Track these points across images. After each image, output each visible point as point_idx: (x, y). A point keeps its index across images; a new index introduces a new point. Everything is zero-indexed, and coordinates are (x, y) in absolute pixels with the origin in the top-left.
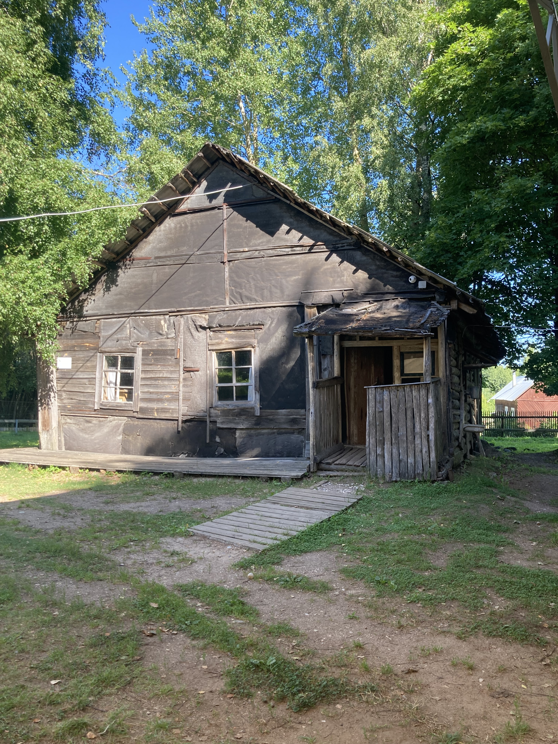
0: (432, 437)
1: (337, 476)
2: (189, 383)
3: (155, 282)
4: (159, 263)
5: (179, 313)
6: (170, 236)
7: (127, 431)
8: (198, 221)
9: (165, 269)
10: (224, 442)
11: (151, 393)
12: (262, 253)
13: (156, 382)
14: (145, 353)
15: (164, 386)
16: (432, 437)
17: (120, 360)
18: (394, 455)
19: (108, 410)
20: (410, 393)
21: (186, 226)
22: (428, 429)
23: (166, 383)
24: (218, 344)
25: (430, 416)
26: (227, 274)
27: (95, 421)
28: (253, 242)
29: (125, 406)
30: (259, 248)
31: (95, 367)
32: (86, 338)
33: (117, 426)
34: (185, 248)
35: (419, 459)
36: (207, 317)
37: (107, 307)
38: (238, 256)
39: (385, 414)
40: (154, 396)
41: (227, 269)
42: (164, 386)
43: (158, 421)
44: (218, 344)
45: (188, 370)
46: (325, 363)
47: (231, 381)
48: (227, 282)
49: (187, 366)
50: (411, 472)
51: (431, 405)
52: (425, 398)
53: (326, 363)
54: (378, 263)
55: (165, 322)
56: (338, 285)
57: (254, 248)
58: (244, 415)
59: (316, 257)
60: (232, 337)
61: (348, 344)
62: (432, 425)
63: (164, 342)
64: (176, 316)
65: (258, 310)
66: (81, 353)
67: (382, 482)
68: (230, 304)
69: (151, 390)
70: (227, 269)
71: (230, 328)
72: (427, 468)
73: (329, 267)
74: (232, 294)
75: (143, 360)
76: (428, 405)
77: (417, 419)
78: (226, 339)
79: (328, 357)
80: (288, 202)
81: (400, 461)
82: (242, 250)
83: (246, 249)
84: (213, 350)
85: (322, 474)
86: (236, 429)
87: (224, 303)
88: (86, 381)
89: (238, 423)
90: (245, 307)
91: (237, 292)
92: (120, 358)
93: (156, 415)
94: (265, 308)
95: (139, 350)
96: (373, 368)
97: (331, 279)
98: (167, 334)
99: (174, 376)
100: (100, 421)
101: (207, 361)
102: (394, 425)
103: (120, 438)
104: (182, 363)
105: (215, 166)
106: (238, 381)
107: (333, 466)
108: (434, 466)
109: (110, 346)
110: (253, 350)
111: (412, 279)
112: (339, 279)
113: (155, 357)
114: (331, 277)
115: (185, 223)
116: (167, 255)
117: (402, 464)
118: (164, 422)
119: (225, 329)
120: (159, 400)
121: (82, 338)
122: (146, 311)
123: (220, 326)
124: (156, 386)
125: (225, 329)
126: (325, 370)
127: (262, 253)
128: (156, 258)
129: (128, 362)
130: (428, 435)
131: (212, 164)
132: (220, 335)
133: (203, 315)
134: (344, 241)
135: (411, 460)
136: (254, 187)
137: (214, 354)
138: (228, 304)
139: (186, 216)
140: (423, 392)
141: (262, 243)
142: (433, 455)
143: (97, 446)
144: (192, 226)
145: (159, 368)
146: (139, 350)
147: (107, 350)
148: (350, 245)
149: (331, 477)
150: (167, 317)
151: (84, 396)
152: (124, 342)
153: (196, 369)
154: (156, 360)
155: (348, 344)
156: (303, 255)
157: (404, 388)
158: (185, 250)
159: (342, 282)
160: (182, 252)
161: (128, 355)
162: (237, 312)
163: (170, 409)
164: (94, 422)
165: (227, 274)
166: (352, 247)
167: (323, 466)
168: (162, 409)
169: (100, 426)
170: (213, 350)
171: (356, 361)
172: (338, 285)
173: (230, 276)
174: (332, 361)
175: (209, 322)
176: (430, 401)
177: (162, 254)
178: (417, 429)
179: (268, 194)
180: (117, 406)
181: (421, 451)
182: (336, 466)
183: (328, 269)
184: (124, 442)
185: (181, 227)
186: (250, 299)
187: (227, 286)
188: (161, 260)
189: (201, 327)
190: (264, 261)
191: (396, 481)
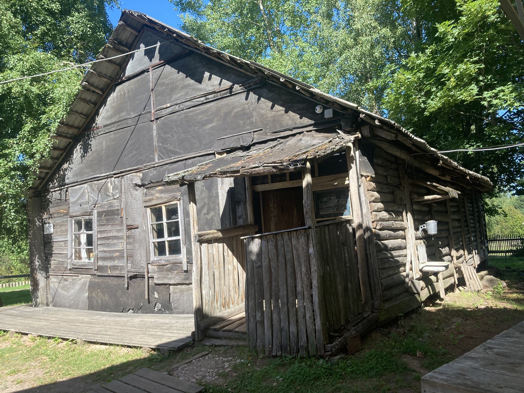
0: (316, 299)
1: (222, 346)
2: (132, 240)
3: (104, 148)
4: (107, 131)
5: (120, 175)
6: (114, 104)
7: (92, 287)
8: (133, 87)
9: (110, 135)
10: (161, 298)
11: (105, 252)
12: (181, 106)
13: (108, 242)
14: (100, 214)
15: (114, 244)
16: (316, 299)
17: (83, 223)
18: (274, 322)
19: (78, 270)
20: (289, 242)
21: (125, 93)
22: (311, 288)
23: (115, 241)
24: (150, 200)
25: (312, 270)
26: (155, 133)
27: (70, 279)
28: (175, 96)
29: (89, 265)
30: (179, 102)
31: (67, 230)
32: (61, 205)
33: (84, 284)
34: (124, 113)
35: (302, 328)
36: (141, 175)
37: (73, 177)
38: (164, 112)
39: (263, 269)
40: (108, 255)
41: (155, 128)
42: (114, 244)
43: (112, 278)
44: (150, 200)
45: (130, 228)
46: (240, 210)
47: (170, 235)
48: (155, 140)
49: (129, 224)
50: (293, 345)
51: (312, 256)
52: (305, 247)
53: (240, 210)
54: (284, 98)
55: (111, 184)
56: (248, 127)
57: (175, 102)
58: (176, 270)
59: (227, 102)
60: (161, 192)
61: (260, 188)
62: (315, 283)
63: (112, 203)
64: (118, 177)
65: (180, 163)
66: (58, 219)
67: (261, 356)
68: (159, 160)
69: (106, 249)
70: (155, 128)
71: (160, 184)
72: (312, 339)
73: (239, 109)
74: (160, 151)
75: (98, 221)
76: (308, 256)
77: (298, 276)
78: (157, 195)
79: (242, 204)
80: (200, 52)
81: (281, 330)
82: (165, 106)
83: (169, 105)
84: (147, 207)
85: (208, 343)
86: (170, 285)
87: (154, 160)
88: (62, 243)
89: (171, 279)
90: (169, 161)
91: (164, 148)
92: (83, 221)
93: (109, 272)
94: (186, 159)
95: (95, 212)
96: (295, 211)
97: (242, 122)
98: (113, 195)
99: (120, 234)
100: (73, 279)
101: (144, 216)
102: (274, 284)
103: (87, 294)
104: (124, 222)
105: (141, 33)
106: (170, 235)
107: (220, 333)
108: (320, 335)
109: (75, 210)
110: (178, 202)
111: (318, 110)
112: (248, 121)
113: (106, 218)
114: (242, 120)
115: (124, 91)
116: (112, 122)
117: (284, 333)
118: (116, 279)
119: (156, 184)
120: (112, 258)
121: (58, 206)
122: (98, 176)
123: (152, 182)
124: (108, 245)
125: (156, 184)
126: (240, 218)
127: (181, 106)
128: (105, 126)
129: (89, 225)
130: (312, 295)
131: (139, 32)
132: (153, 191)
133: (138, 174)
134: (250, 81)
135: (293, 329)
136: (172, 45)
137: (149, 210)
138: (157, 161)
139: (124, 84)
140: (302, 240)
141: (181, 96)
142: (318, 322)
143: (73, 302)
144: (128, 92)
145: (109, 228)
146: (95, 212)
147: (74, 214)
148: (256, 84)
149: (216, 346)
150: (113, 179)
151: (62, 257)
152: (85, 206)
153: (135, 226)
154: (107, 220)
155: (260, 188)
156: (215, 102)
157: (282, 236)
158: (124, 114)
159: (252, 123)
160: (122, 117)
161: (87, 217)
162: (164, 167)
163: (119, 266)
164: (69, 280)
165: (155, 133)
166: (259, 85)
167: (211, 332)
168: (113, 266)
169: (74, 284)
170: (147, 207)
171: (275, 206)
172: (248, 127)
173: (158, 134)
174: (245, 208)
175: (142, 180)
176: (311, 250)
177: (108, 123)
178: (299, 288)
179: (184, 48)
180: (83, 265)
181: (305, 316)
182: (224, 333)
183: (238, 112)
184: (89, 298)
185: (121, 95)
186: (176, 153)
187: (155, 143)
188: (108, 127)
189: (136, 185)
190: (184, 114)
191: (276, 356)
